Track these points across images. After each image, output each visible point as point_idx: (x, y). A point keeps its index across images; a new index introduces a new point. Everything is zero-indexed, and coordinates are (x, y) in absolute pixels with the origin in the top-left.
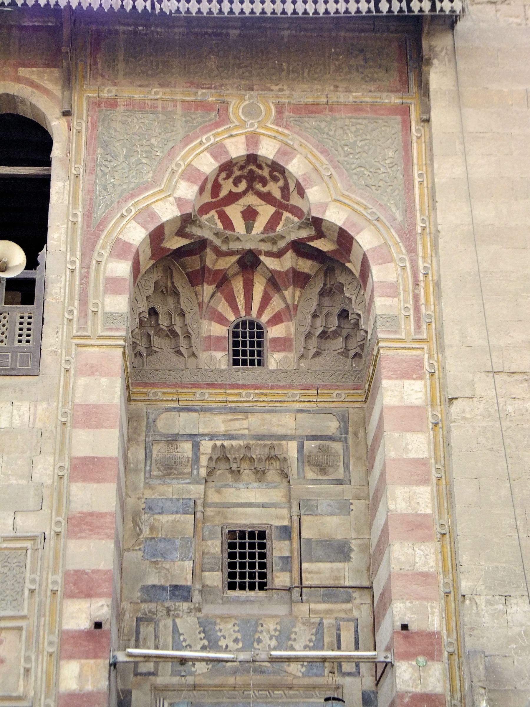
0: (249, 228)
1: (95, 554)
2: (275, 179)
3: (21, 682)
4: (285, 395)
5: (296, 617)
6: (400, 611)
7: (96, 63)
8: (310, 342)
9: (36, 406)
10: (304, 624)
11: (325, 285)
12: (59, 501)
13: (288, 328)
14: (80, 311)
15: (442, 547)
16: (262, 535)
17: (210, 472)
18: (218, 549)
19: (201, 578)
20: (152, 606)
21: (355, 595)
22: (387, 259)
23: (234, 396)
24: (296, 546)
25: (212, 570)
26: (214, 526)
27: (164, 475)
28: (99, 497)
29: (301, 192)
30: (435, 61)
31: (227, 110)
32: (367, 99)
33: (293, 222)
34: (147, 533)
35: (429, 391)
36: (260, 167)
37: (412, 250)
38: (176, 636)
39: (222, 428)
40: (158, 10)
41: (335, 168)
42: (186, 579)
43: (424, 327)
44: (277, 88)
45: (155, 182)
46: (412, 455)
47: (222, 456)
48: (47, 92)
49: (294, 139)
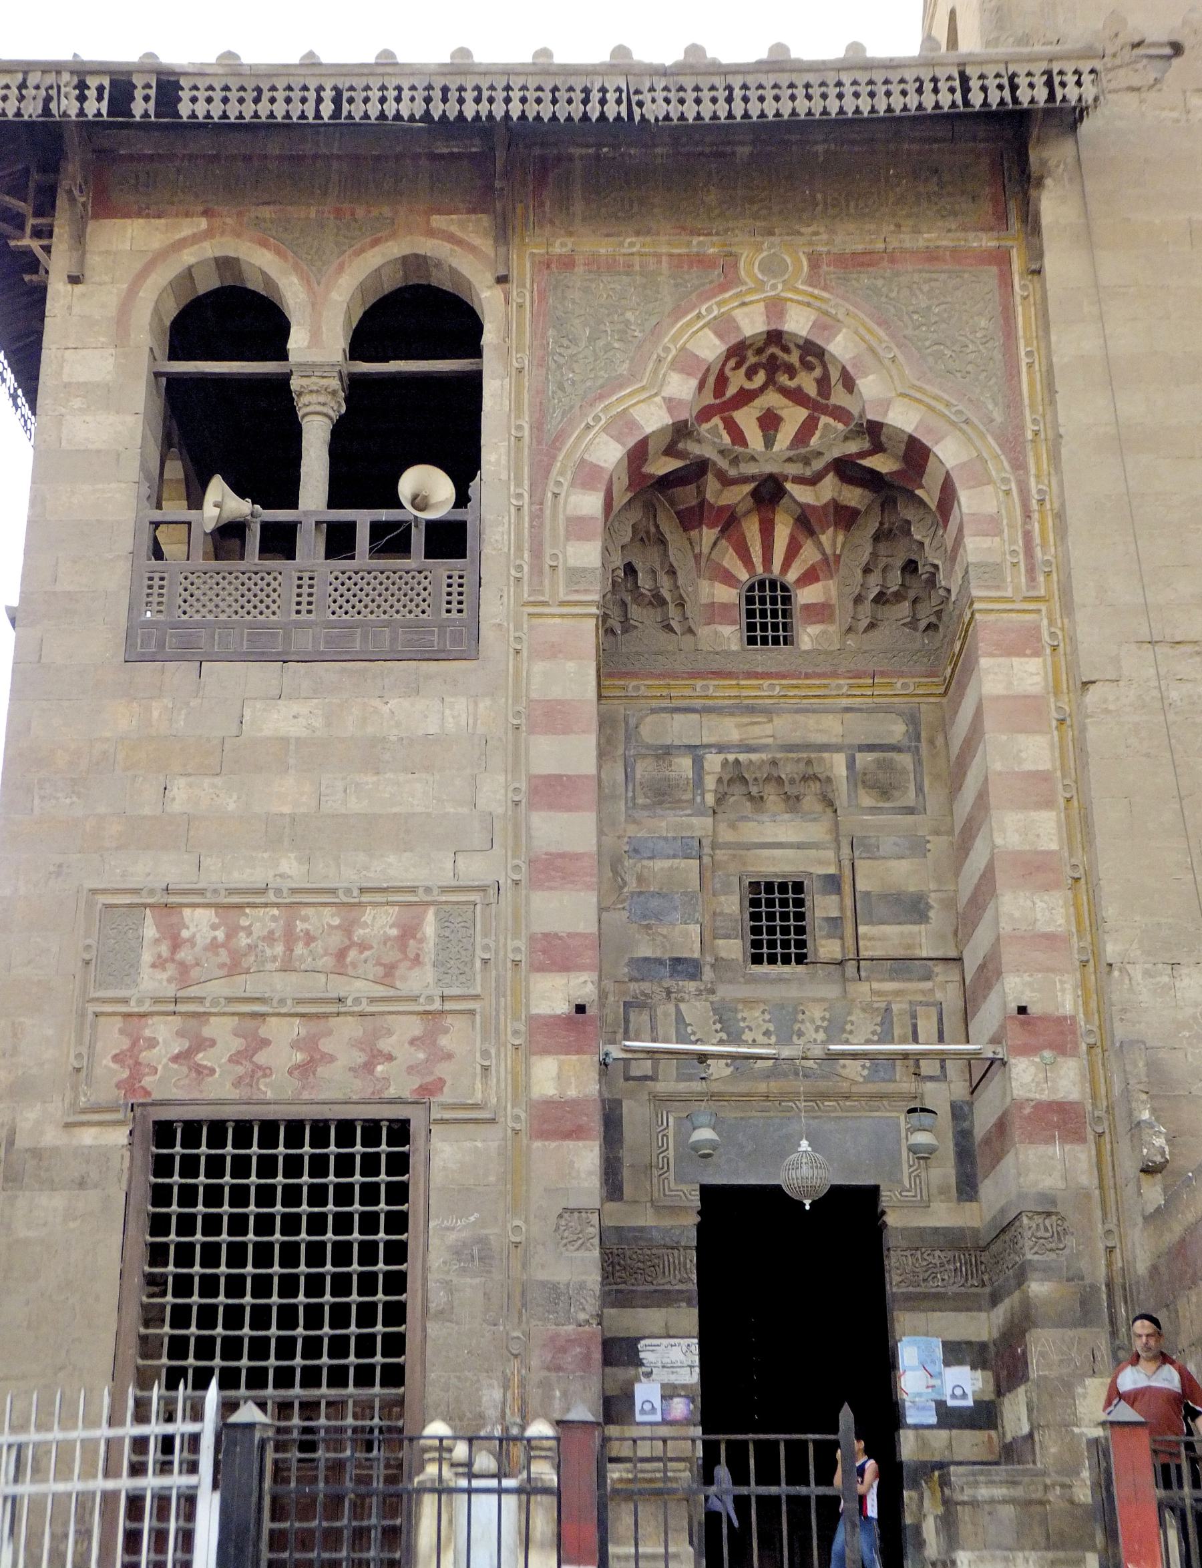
0: (769, 442)
1: (571, 911)
2: (809, 367)
3: (478, 1085)
4: (825, 686)
5: (853, 1001)
6: (1015, 987)
7: (542, 204)
8: (860, 608)
9: (476, 704)
10: (864, 1010)
11: (881, 524)
12: (516, 837)
13: (827, 590)
14: (532, 567)
15: (1075, 896)
16: (798, 887)
17: (719, 801)
18: (736, 908)
19: (713, 948)
20: (646, 986)
21: (936, 970)
22: (982, 479)
23: (752, 690)
24: (849, 902)
25: (727, 937)
26: (728, 876)
27: (654, 804)
28: (572, 831)
29: (849, 384)
30: (1048, 182)
31: (735, 266)
32: (945, 243)
33: (836, 430)
34: (632, 885)
35: (1050, 670)
36: (786, 350)
37: (1019, 465)
38: (682, 1026)
39: (735, 736)
40: (637, 118)
41: (899, 346)
42: (692, 950)
43: (1041, 578)
44: (810, 230)
45: (633, 376)
46: (1028, 766)
47: (736, 776)
48: (473, 249)
49: (838, 306)
